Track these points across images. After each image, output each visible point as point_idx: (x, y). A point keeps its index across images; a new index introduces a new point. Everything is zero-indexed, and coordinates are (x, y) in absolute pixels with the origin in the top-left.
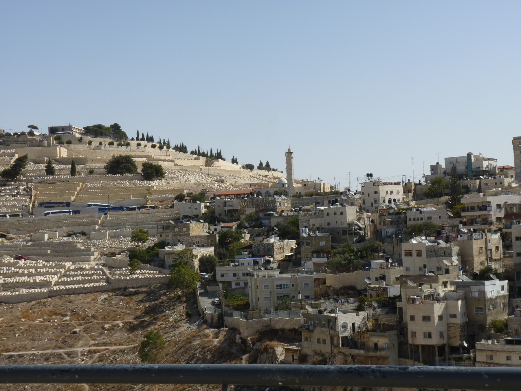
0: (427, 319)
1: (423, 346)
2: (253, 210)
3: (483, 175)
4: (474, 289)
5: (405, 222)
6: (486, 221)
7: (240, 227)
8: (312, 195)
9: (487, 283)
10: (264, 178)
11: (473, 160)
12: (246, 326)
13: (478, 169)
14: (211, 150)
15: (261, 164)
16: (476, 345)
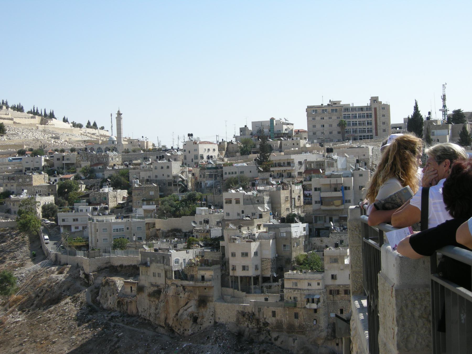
0: (245, 255)
1: (241, 277)
2: (88, 164)
3: (282, 137)
4: (283, 230)
5: (222, 176)
6: (290, 176)
7: (77, 178)
8: (138, 152)
9: (293, 225)
10: (93, 136)
11: (275, 123)
12: (88, 264)
13: (279, 132)
14: (45, 110)
15: (89, 123)
16: (285, 275)
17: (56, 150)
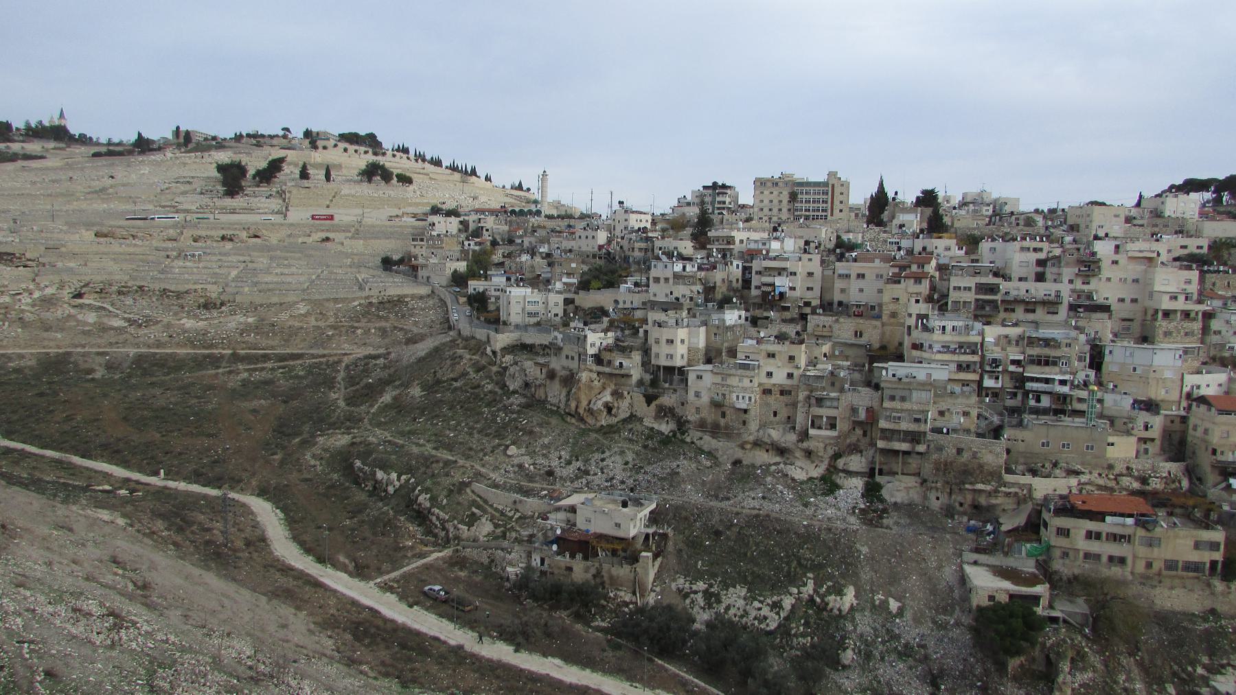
1: (665, 367)
17: (435, 210)
